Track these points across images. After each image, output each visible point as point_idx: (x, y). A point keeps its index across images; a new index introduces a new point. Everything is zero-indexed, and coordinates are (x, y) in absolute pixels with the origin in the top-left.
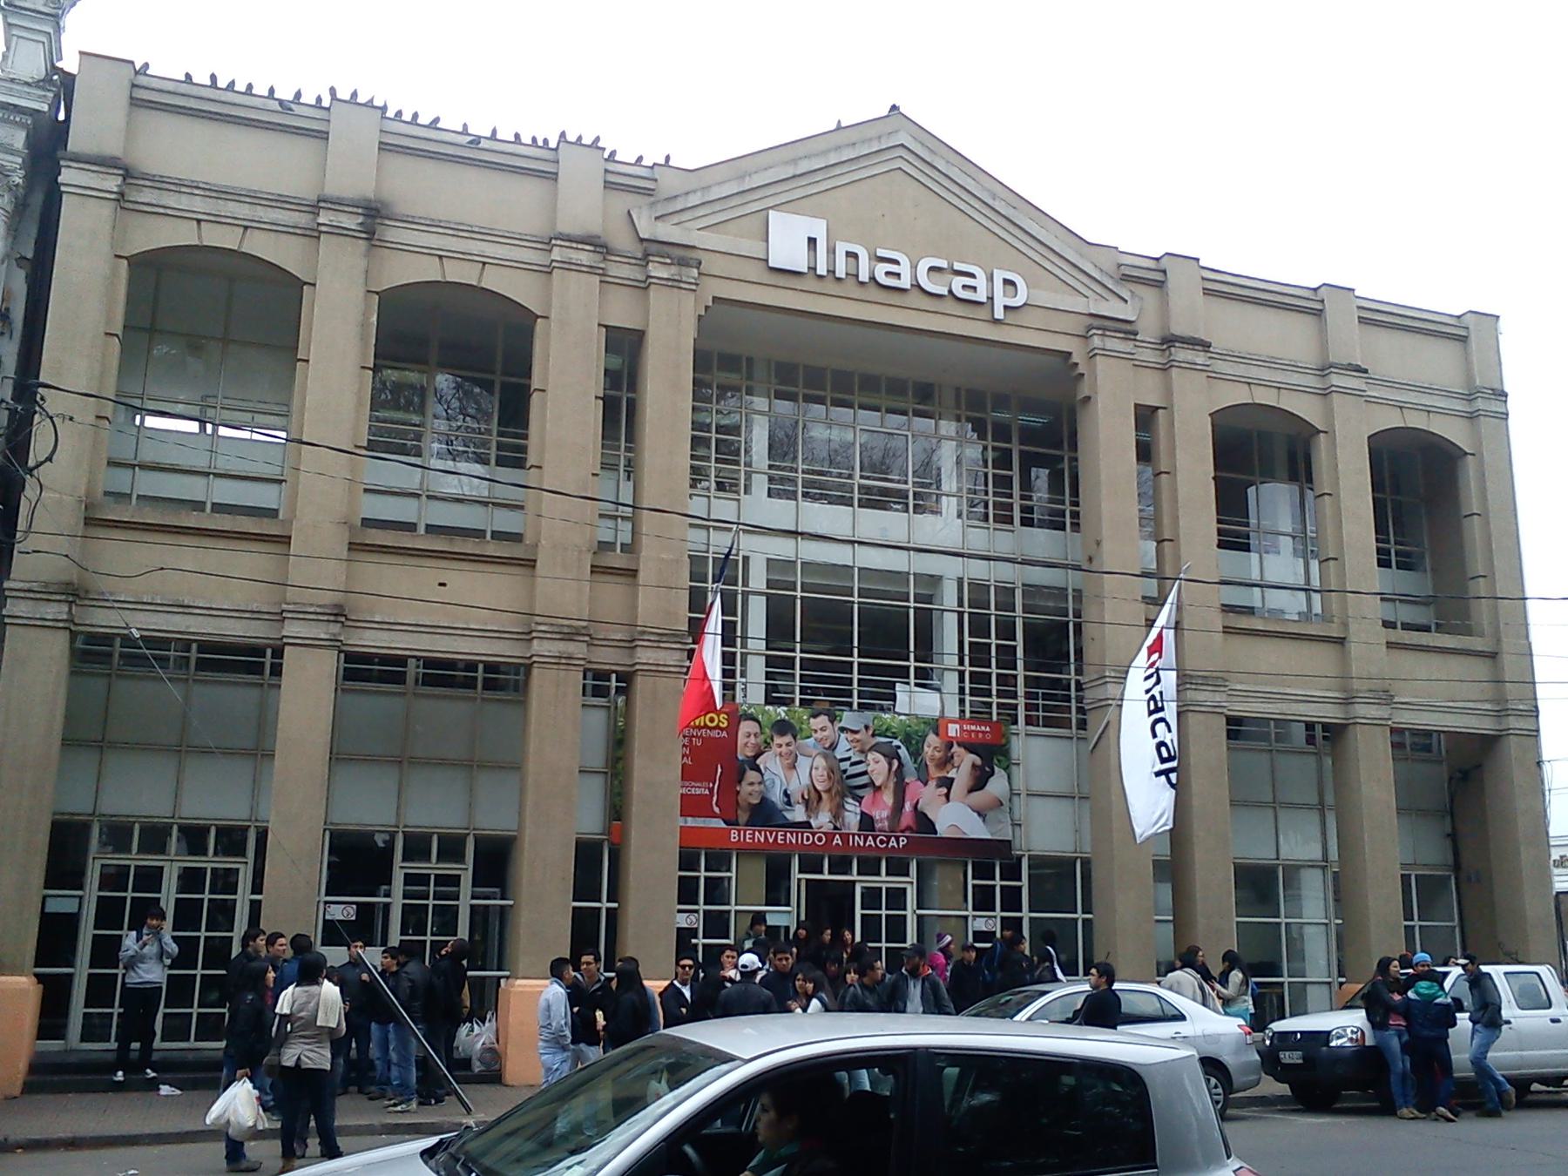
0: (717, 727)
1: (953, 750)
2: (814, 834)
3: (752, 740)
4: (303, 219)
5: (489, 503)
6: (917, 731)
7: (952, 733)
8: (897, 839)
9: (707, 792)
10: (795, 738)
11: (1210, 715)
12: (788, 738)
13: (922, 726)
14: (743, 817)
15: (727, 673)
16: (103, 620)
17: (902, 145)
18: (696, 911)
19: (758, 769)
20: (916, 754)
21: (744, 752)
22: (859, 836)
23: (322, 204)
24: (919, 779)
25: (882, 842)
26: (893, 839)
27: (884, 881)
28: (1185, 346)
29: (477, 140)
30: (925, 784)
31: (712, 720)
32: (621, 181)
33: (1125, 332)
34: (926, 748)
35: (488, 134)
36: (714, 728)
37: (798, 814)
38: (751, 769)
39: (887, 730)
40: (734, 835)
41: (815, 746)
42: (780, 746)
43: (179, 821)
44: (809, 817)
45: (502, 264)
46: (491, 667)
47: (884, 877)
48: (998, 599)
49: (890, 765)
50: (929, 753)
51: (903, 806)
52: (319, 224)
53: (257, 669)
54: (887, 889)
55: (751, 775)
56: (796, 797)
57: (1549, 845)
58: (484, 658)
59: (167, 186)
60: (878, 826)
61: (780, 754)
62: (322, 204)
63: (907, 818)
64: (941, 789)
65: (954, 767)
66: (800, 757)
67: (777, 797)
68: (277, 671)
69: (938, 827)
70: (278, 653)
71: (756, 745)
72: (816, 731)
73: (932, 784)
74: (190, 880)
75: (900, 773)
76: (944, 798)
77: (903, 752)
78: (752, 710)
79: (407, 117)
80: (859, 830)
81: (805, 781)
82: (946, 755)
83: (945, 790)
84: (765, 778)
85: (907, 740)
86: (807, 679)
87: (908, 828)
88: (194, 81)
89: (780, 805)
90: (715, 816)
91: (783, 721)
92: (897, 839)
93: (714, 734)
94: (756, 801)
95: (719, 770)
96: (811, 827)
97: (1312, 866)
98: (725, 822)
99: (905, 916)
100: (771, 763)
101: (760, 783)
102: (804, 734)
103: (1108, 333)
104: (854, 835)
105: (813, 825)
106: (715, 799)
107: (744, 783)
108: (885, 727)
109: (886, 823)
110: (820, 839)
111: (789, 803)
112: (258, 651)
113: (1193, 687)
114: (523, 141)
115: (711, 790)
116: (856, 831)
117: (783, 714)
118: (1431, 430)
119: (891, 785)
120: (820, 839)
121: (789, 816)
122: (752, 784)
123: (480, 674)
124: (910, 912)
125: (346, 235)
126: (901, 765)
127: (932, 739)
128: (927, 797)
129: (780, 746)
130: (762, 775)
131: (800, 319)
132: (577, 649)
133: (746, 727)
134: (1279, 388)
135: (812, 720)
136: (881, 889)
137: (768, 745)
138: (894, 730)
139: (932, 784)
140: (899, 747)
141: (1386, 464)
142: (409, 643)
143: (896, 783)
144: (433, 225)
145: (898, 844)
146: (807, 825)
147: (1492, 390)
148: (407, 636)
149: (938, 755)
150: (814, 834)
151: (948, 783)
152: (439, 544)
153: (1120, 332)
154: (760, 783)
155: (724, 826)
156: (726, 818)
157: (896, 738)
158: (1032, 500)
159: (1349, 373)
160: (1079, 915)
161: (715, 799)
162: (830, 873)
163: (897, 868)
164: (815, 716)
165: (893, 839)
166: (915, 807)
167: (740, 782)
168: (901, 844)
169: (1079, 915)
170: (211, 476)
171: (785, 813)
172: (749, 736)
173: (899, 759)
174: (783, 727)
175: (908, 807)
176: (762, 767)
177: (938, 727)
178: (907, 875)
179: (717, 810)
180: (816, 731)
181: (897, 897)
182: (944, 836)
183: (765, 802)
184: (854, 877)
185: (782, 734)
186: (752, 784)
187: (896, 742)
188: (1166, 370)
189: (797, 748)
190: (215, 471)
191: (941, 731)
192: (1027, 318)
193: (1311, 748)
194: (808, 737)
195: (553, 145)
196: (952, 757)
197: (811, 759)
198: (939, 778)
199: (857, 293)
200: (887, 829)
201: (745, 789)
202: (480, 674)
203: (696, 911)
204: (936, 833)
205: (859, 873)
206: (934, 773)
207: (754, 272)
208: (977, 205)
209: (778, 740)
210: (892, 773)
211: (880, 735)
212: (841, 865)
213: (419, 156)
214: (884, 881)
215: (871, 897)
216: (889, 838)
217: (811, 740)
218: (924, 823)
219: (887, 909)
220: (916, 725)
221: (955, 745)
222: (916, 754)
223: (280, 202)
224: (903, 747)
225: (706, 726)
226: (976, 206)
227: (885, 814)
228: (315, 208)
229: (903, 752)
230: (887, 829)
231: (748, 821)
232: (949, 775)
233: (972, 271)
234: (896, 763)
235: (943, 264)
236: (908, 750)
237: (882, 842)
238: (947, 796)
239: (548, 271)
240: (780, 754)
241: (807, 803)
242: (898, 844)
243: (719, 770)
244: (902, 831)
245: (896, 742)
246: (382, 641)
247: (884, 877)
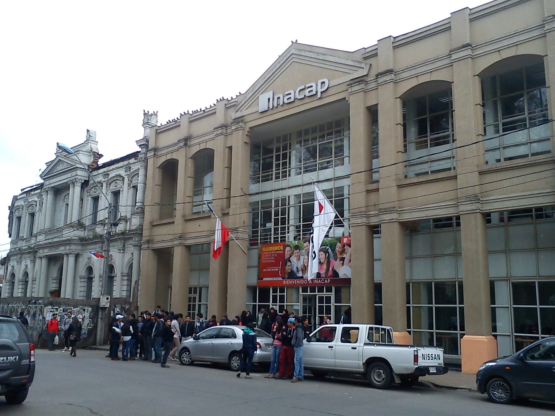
0: (281, 250)
1: (345, 248)
2: (304, 280)
3: (289, 252)
4: (447, 61)
5: (451, 157)
6: (334, 243)
7: (345, 242)
8: (327, 280)
9: (278, 270)
10: (300, 250)
11: (389, 223)
12: (298, 251)
13: (336, 240)
14: (287, 276)
15: (299, 231)
16: (189, 242)
17: (292, 54)
18: (277, 305)
19: (290, 261)
20: (333, 250)
21: (287, 256)
22: (316, 280)
23: (451, 53)
24: (334, 259)
25: (323, 281)
26: (326, 280)
27: (325, 294)
28: (382, 76)
29: (204, 111)
30: (336, 260)
31: (279, 248)
32: (422, 36)
33: (358, 82)
34: (336, 248)
35: (205, 109)
36: (280, 250)
37: (300, 274)
38: (289, 262)
39: (325, 243)
40: (284, 282)
41: (305, 252)
42: (296, 253)
43: (459, 280)
44: (303, 275)
45: (436, 69)
46: (539, 209)
47: (325, 293)
48: (275, 204)
49: (326, 255)
50: (338, 250)
51: (329, 269)
52: (545, 31)
53: (451, 225)
54: (326, 297)
55: (289, 263)
56: (300, 269)
57: (87, 282)
58: (454, 215)
59: (400, 72)
60: (322, 276)
61: (296, 256)
62: (451, 53)
63: (330, 273)
64: (341, 262)
65: (345, 253)
66: (301, 256)
67: (295, 269)
68: (458, 224)
69: (339, 275)
70: (458, 218)
71: (290, 254)
72: (305, 247)
73: (338, 260)
74: (321, 299)
75: (328, 258)
76: (342, 265)
77: (330, 250)
78: (289, 243)
79: (199, 110)
80: (317, 278)
81: (302, 264)
82: (342, 250)
83: (342, 262)
84: (292, 263)
85: (331, 247)
86: (283, 233)
87: (331, 276)
88: (242, 93)
89: (296, 272)
90: (280, 277)
91: (297, 245)
92: (327, 280)
93: (279, 252)
94: (289, 271)
95: (281, 263)
96: (303, 278)
97: (502, 280)
98: (283, 278)
99: (330, 306)
100: (294, 259)
101: (291, 266)
102: (302, 249)
103: (352, 85)
104: (315, 280)
105: (304, 277)
106: (280, 271)
107: (287, 266)
108: (324, 243)
109: (324, 275)
110: (306, 282)
111: (298, 271)
112: (450, 219)
113: (381, 213)
114: (208, 108)
115: (279, 269)
116: (315, 278)
117: (297, 243)
118: (420, 83)
119: (326, 262)
120: (306, 282)
121: (298, 275)
122: (289, 266)
123: (534, 213)
124: (333, 304)
125: (461, 60)
126: (329, 255)
127: (339, 245)
128: (336, 265)
129: (296, 253)
130: (291, 263)
131: (277, 122)
132: (395, 216)
133: (288, 249)
134: (417, 76)
135: (304, 244)
136: (323, 297)
137: (293, 253)
138: (327, 243)
139: (338, 260)
140: (328, 249)
141: (427, 100)
142: (418, 216)
143: (327, 261)
144: (487, 44)
145: (327, 281)
146: (302, 277)
147: (553, 16)
148: (194, 240)
149: (340, 250)
150: (304, 280)
151: (343, 259)
152: (422, 179)
153: (356, 83)
154: (291, 266)
155: (282, 279)
156: (283, 277)
157: (327, 246)
158: (535, 113)
159: (460, 50)
160: (411, 305)
161: (280, 271)
162: (310, 292)
163: (329, 290)
164: (305, 242)
165: (326, 280)
166: (333, 268)
167: (286, 266)
168: (328, 281)
169: (458, 305)
170: (429, 162)
171: (297, 274)
172: (288, 252)
173: (328, 253)
174: (297, 247)
175: (331, 269)
176: (291, 261)
177: (340, 240)
178: (332, 292)
179: (280, 275)
180: (305, 247)
181: (328, 299)
182: (341, 278)
183: (292, 271)
184: (316, 293)
185: (296, 249)
186: (289, 266)
187: (328, 247)
188: (365, 92)
189: (300, 253)
190: (530, 141)
191: (342, 241)
192: (330, 92)
193: (502, 224)
194: (303, 249)
195: (179, 118)
196: (345, 250)
197: (303, 256)
198: (340, 258)
199: (282, 109)
200: (324, 277)
201: (287, 268)
202: (534, 213)
203: (276, 305)
204: (339, 277)
205: (318, 292)
206: (339, 256)
207: (256, 116)
208: (314, 60)
209: (295, 252)
210: (326, 258)
211: (323, 246)
212: (313, 290)
213: (406, 45)
214: (325, 294)
215: (321, 299)
216: (325, 280)
217: (304, 250)
218: (336, 274)
219: (326, 303)
220: (334, 241)
221: (346, 246)
222: (333, 250)
223: (438, 59)
224: (330, 249)
225: (278, 250)
226: (315, 61)
227: (324, 272)
228: (543, 26)
229: (330, 250)
230: (324, 277)
231: (288, 277)
232: (344, 256)
233: (311, 85)
234: (327, 254)
235: (303, 87)
236: (331, 249)
237: (323, 281)
238: (343, 264)
239: (544, 36)
240: (296, 256)
241: (302, 270)
242: (327, 281)
243: (281, 263)
244: (329, 277)
245: (328, 247)
246: (421, 215)
247: (325, 293)
